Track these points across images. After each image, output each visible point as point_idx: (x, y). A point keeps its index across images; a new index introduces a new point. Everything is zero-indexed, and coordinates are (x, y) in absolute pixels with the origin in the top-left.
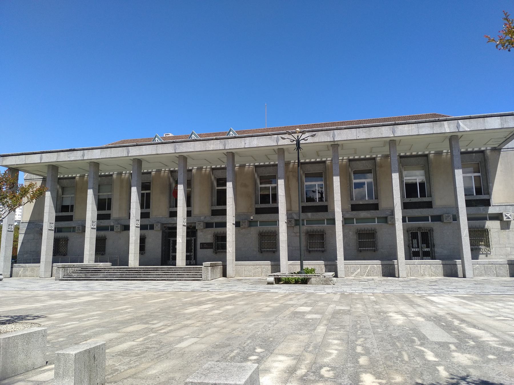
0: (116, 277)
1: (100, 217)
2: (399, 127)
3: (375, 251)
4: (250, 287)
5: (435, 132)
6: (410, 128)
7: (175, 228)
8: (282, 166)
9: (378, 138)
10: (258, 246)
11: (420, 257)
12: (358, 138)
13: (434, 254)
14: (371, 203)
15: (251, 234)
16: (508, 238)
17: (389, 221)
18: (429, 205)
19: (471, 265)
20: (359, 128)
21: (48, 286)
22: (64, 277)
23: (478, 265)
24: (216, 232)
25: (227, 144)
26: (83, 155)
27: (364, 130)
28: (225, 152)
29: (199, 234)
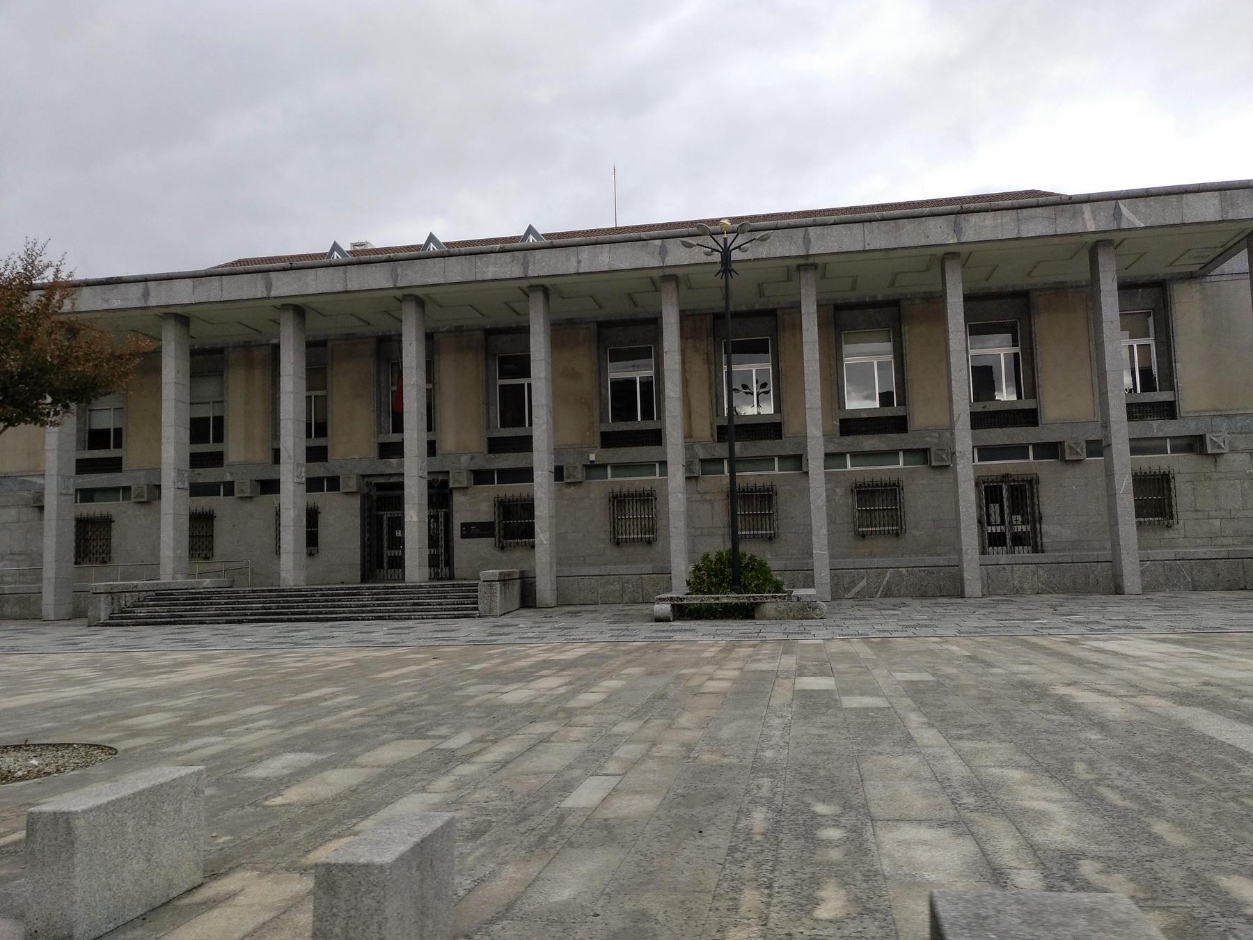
0: (251, 615)
1: (197, 461)
2: (971, 218)
3: (897, 535)
4: (615, 630)
5: (1060, 231)
6: (999, 221)
7: (401, 486)
8: (672, 321)
9: (916, 247)
10: (608, 527)
11: (1006, 546)
12: (868, 248)
13: (1041, 539)
14: (889, 414)
15: (591, 499)
16: (1216, 497)
17: (933, 459)
18: (1030, 417)
19: (1137, 562)
20: (870, 221)
21: (76, 641)
22: (111, 618)
23: (1148, 563)
24: (502, 495)
25: (531, 264)
26: (146, 295)
27: (882, 227)
28: (525, 284)
29: (458, 499)
